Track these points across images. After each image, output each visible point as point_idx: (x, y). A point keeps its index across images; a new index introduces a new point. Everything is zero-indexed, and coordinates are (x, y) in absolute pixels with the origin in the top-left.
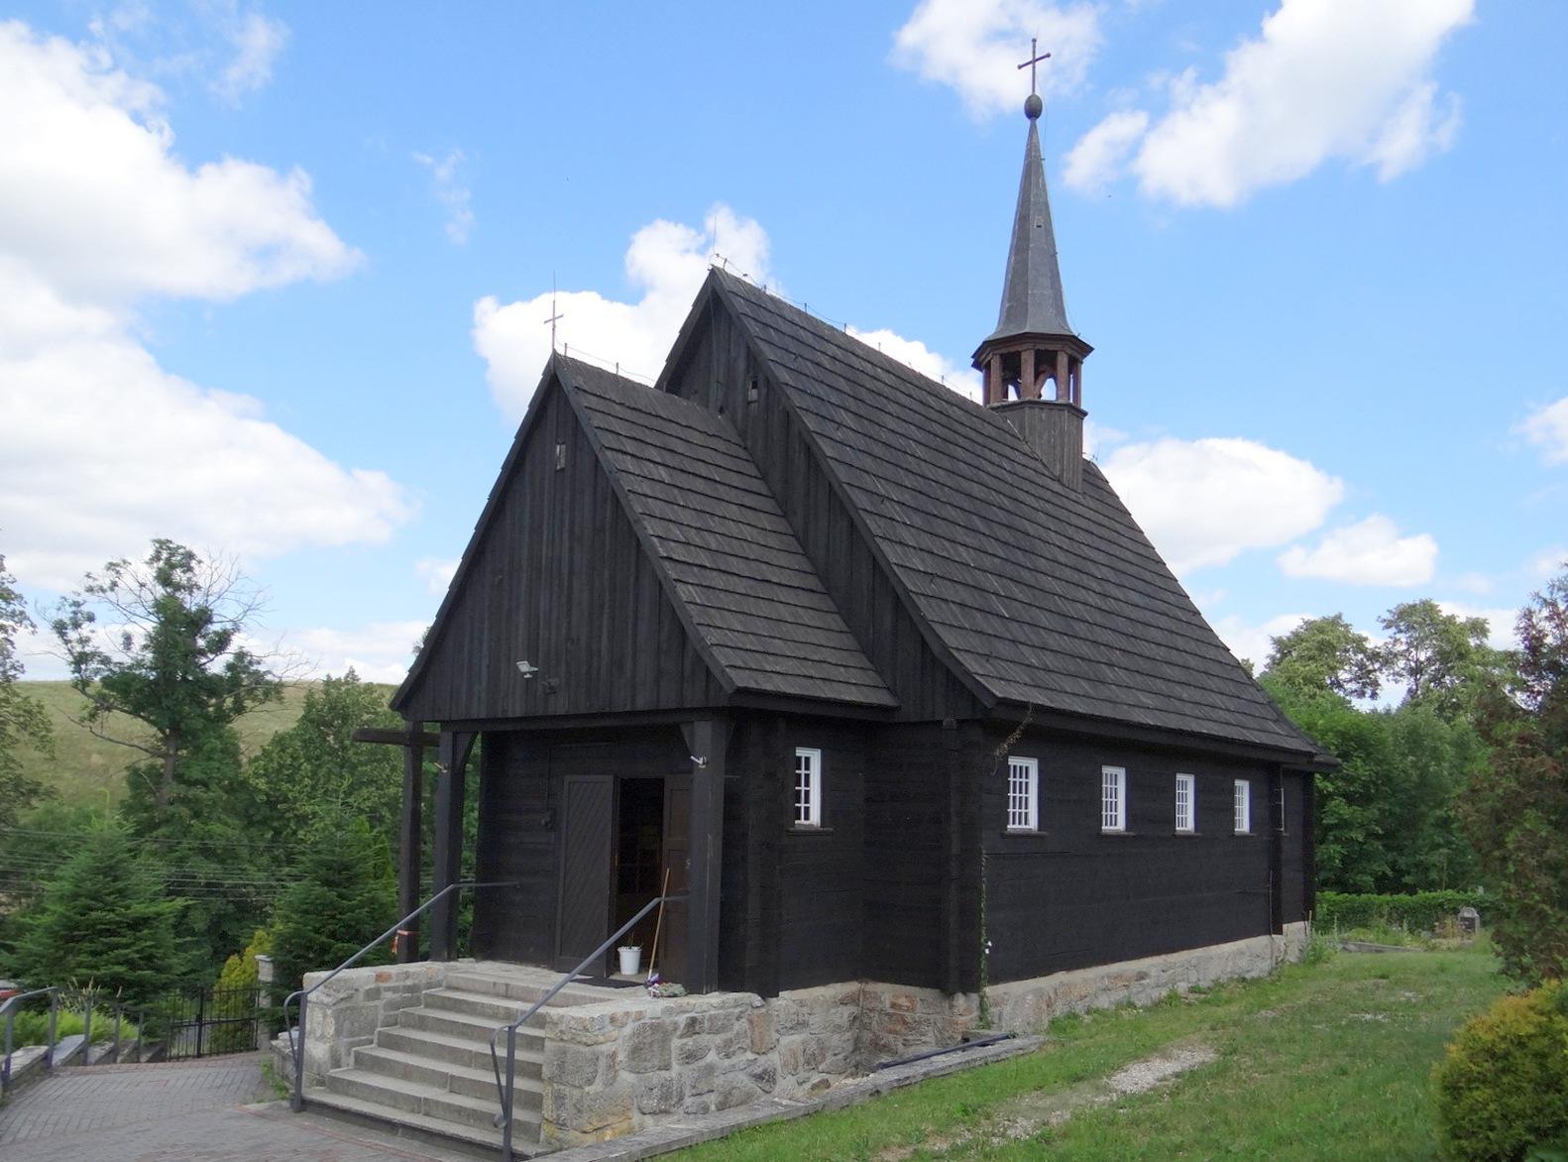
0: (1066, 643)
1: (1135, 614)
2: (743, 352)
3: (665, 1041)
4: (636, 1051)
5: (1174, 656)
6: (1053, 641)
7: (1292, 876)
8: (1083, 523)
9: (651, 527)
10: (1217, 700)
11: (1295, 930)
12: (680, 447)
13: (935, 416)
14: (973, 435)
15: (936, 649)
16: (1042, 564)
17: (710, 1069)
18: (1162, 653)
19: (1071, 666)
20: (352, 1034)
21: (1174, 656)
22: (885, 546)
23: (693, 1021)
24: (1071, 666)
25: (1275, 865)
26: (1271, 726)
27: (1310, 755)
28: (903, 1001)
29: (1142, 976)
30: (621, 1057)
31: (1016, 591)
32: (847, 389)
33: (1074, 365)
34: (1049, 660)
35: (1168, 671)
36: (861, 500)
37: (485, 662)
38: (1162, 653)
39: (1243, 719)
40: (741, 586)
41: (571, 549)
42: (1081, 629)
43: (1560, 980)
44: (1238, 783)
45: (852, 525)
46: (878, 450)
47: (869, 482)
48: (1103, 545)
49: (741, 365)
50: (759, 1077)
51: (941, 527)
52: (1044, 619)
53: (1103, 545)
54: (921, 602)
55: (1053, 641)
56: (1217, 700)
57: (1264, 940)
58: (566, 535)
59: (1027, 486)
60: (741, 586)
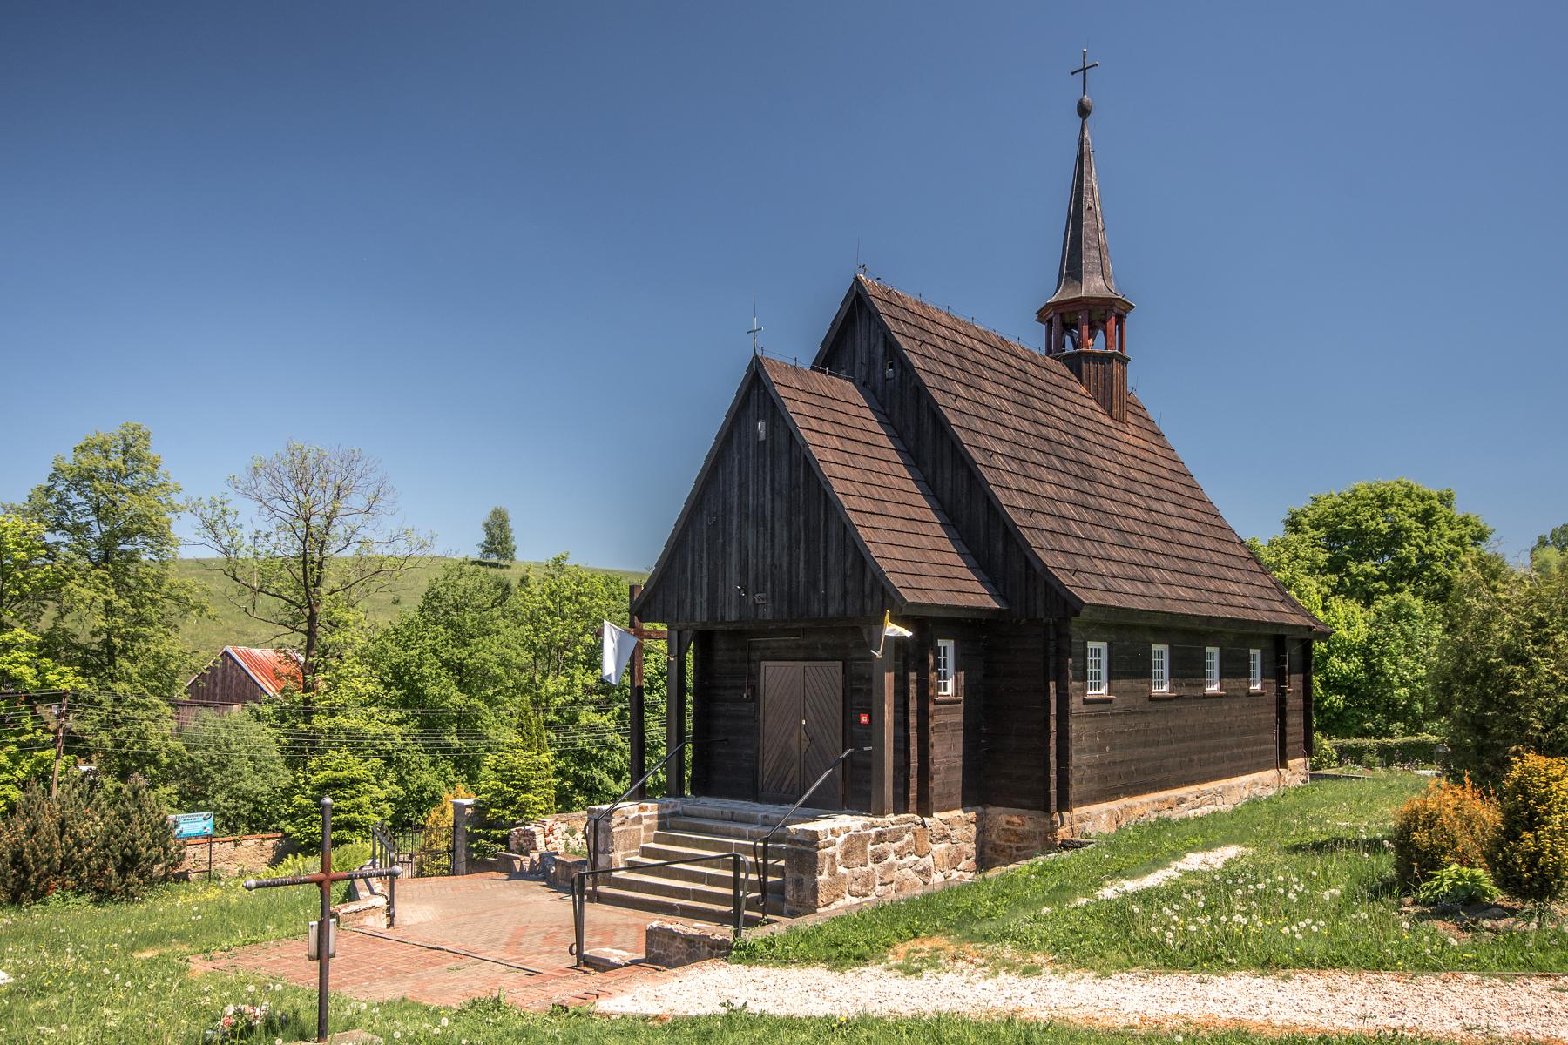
0: (1125, 554)
1: (1174, 523)
2: (881, 339)
3: (864, 846)
4: (846, 854)
5: (1203, 555)
6: (1115, 553)
7: (1295, 722)
8: (1128, 449)
9: (837, 486)
10: (1234, 587)
11: (1297, 764)
12: (844, 419)
13: (1017, 374)
14: (1045, 385)
15: (1038, 567)
16: (1102, 489)
17: (891, 866)
18: (1194, 553)
19: (1129, 570)
20: (625, 849)
21: (1203, 555)
22: (998, 492)
23: (880, 834)
24: (1129, 570)
25: (1282, 714)
26: (1277, 606)
27: (1310, 628)
28: (1015, 819)
29: (1181, 801)
30: (838, 857)
31: (1087, 516)
32: (956, 363)
33: (1120, 319)
34: (1115, 569)
35: (1200, 568)
36: (978, 456)
37: (705, 580)
38: (1194, 553)
39: (1257, 603)
40: (898, 525)
41: (773, 500)
42: (1133, 540)
43: (42, 634)
44: (1252, 651)
45: (970, 471)
46: (983, 412)
47: (983, 441)
48: (1146, 467)
49: (880, 350)
50: (921, 872)
51: (1032, 470)
52: (1106, 535)
53: (1146, 467)
54: (1026, 533)
55: (1115, 553)
56: (1234, 587)
57: (1272, 773)
58: (768, 489)
59: (1085, 424)
60: (898, 525)
